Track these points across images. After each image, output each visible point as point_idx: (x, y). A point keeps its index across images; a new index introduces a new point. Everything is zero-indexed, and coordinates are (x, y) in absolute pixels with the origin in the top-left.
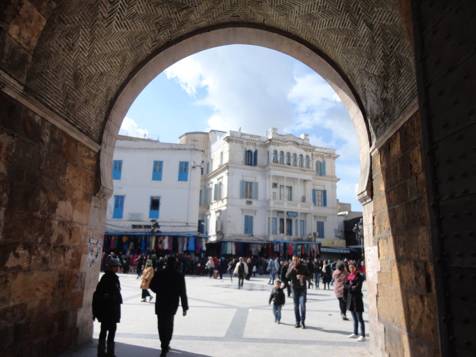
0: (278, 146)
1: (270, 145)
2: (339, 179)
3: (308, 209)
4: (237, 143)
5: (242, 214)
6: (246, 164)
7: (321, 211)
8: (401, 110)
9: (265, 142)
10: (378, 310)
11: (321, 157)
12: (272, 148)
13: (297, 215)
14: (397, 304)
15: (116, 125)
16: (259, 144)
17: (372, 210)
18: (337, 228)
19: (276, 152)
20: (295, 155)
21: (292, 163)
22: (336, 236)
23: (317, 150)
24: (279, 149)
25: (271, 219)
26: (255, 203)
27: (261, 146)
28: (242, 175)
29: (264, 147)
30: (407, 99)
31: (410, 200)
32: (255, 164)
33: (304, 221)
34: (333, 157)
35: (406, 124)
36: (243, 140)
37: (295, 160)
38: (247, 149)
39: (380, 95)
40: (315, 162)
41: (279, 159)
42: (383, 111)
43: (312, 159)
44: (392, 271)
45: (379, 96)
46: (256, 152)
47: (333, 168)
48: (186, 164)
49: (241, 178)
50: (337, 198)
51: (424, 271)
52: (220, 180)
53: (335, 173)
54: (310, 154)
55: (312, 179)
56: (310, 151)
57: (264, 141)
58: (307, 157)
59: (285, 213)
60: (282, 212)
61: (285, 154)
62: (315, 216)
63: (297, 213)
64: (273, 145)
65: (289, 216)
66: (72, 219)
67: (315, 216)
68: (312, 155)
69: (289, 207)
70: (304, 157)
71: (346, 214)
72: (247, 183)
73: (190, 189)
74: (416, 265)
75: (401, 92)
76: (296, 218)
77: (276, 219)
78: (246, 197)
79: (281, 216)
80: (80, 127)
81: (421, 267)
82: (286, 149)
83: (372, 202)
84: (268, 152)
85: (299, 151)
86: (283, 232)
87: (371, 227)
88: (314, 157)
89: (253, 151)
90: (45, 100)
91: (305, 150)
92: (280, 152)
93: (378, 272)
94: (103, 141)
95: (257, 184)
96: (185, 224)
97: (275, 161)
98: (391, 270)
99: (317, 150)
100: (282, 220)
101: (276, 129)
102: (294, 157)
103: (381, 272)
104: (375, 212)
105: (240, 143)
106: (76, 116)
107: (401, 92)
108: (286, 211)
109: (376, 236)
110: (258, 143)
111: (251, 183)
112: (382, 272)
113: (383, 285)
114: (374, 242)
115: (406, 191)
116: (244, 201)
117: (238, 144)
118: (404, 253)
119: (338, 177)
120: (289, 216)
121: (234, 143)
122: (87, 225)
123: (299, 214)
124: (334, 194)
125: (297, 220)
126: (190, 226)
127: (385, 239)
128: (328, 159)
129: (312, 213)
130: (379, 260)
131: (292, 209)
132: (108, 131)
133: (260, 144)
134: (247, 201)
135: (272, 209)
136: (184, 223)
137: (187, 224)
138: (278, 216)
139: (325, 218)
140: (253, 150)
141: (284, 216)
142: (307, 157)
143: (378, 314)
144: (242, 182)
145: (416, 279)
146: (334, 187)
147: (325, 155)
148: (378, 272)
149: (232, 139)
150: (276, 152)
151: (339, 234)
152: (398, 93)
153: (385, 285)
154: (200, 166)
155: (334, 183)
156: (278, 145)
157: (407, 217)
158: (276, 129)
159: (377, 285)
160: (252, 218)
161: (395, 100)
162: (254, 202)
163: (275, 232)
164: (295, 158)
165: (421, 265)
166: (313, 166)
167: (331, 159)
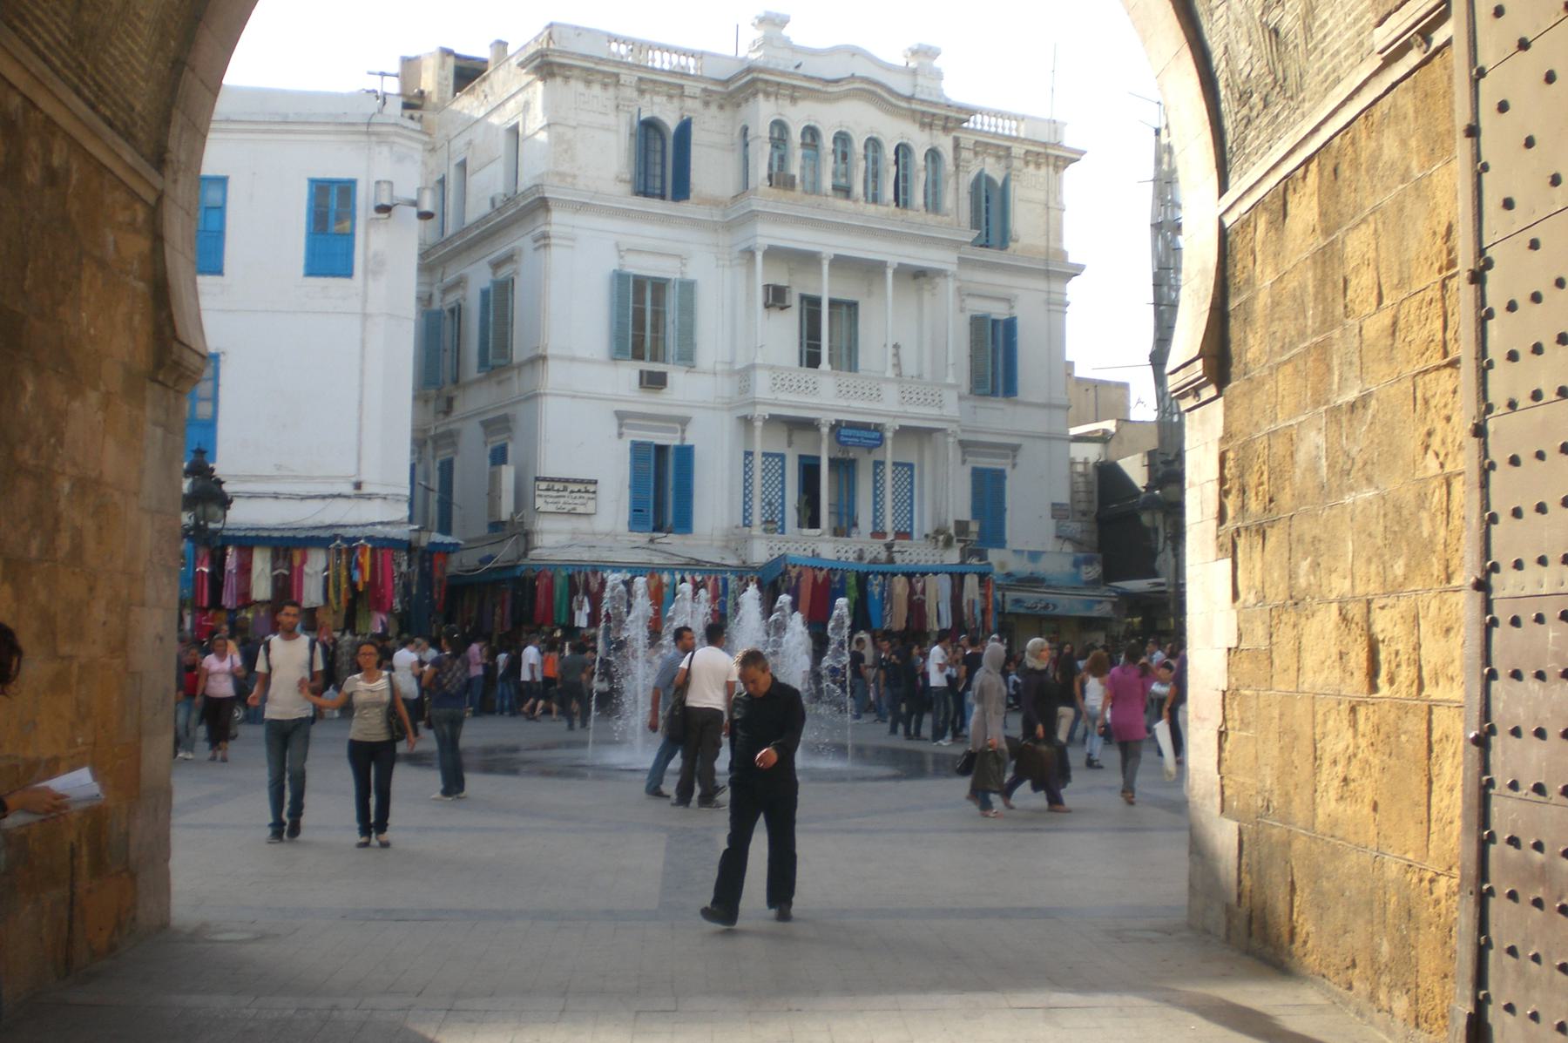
0: (793, 100)
1: (755, 95)
2: (1077, 270)
3: (934, 412)
4: (588, 83)
5: (620, 435)
6: (637, 193)
7: (997, 419)
8: (1326, 85)
9: (726, 82)
10: (1222, 778)
11: (998, 158)
12: (764, 112)
13: (881, 439)
14: (1281, 748)
15: (207, 87)
16: (698, 92)
17: (1220, 433)
18: (1064, 497)
19: (780, 127)
20: (874, 144)
21: (858, 188)
22: (1058, 537)
23: (976, 122)
24: (798, 116)
25: (758, 461)
26: (684, 388)
27: (707, 98)
28: (617, 245)
29: (721, 107)
30: (1343, 54)
31: (1339, 402)
32: (681, 189)
33: (911, 466)
34: (1057, 157)
35: (1337, 139)
36: (623, 71)
37: (874, 175)
38: (644, 116)
39: (1260, 12)
40: (967, 180)
41: (795, 169)
42: (1270, 73)
43: (957, 167)
44: (1274, 639)
45: (1258, 14)
46: (685, 128)
47: (1051, 209)
48: (346, 189)
49: (613, 264)
50: (1068, 358)
51: (1365, 627)
52: (504, 272)
53: (1059, 238)
54: (945, 143)
55: (952, 268)
56: (945, 129)
57: (724, 77)
58: (933, 155)
59: (825, 430)
60: (809, 425)
61: (827, 142)
62: (964, 445)
63: (878, 428)
64: (767, 95)
65: (844, 444)
66: (101, 473)
67: (964, 445)
68: (957, 146)
69: (843, 403)
70: (919, 157)
71: (1105, 432)
72: (640, 283)
73: (365, 316)
74: (1344, 612)
75: (1325, 22)
76: (877, 455)
77: (782, 457)
78: (638, 355)
79: (803, 445)
80: (108, 113)
81: (1357, 618)
82: (830, 118)
83: (1221, 400)
84: (745, 130)
85: (893, 131)
86: (814, 522)
87: (1213, 489)
88: (965, 154)
89: (671, 122)
90: (31, 28)
91: (923, 125)
92: (803, 135)
93: (1229, 649)
94: (168, 156)
95: (688, 288)
96: (348, 489)
97: (780, 179)
98: (1271, 637)
99: (976, 122)
100: (809, 471)
101: (782, 22)
102: (870, 154)
103: (1237, 648)
104: (1227, 436)
105: (605, 86)
106: (99, 72)
107: (1325, 22)
108: (827, 419)
109: (1230, 525)
110: (692, 88)
111: (660, 286)
112: (1241, 648)
113: (1243, 692)
114: (1220, 547)
115: (1329, 369)
116: (630, 371)
117: (596, 89)
118: (1312, 578)
119: (1072, 259)
120: (844, 444)
121: (577, 86)
122: (136, 494)
123: (889, 435)
124: (1055, 338)
125: (878, 464)
126: (370, 497)
127: (1257, 531)
128: (1032, 167)
129: (951, 427)
130: (1234, 608)
131: (858, 408)
132: (183, 113)
133: (705, 90)
134: (641, 372)
135: (763, 411)
136: (346, 478)
137: (358, 486)
138: (790, 444)
139: (1015, 449)
140: (671, 121)
141: (819, 447)
142: (933, 155)
143: (1223, 793)
144: (620, 278)
145: (1341, 655)
146: (1058, 306)
147: (1018, 150)
148: (1229, 649)
149: (562, 66)
150: (780, 127)
151: (1074, 527)
152: (1317, 24)
153: (1247, 692)
154: (414, 204)
155: (1055, 286)
156: (795, 93)
157: (1327, 459)
158: (782, 22)
159: (1224, 692)
160: (998, 477)
161: (1307, 44)
162: (677, 377)
163: (773, 525)
164: (875, 162)
165: (1356, 611)
166: (957, 199)
167: (1043, 171)
